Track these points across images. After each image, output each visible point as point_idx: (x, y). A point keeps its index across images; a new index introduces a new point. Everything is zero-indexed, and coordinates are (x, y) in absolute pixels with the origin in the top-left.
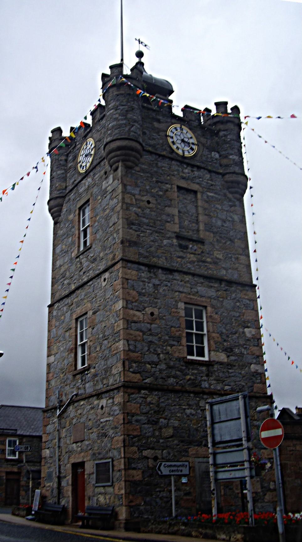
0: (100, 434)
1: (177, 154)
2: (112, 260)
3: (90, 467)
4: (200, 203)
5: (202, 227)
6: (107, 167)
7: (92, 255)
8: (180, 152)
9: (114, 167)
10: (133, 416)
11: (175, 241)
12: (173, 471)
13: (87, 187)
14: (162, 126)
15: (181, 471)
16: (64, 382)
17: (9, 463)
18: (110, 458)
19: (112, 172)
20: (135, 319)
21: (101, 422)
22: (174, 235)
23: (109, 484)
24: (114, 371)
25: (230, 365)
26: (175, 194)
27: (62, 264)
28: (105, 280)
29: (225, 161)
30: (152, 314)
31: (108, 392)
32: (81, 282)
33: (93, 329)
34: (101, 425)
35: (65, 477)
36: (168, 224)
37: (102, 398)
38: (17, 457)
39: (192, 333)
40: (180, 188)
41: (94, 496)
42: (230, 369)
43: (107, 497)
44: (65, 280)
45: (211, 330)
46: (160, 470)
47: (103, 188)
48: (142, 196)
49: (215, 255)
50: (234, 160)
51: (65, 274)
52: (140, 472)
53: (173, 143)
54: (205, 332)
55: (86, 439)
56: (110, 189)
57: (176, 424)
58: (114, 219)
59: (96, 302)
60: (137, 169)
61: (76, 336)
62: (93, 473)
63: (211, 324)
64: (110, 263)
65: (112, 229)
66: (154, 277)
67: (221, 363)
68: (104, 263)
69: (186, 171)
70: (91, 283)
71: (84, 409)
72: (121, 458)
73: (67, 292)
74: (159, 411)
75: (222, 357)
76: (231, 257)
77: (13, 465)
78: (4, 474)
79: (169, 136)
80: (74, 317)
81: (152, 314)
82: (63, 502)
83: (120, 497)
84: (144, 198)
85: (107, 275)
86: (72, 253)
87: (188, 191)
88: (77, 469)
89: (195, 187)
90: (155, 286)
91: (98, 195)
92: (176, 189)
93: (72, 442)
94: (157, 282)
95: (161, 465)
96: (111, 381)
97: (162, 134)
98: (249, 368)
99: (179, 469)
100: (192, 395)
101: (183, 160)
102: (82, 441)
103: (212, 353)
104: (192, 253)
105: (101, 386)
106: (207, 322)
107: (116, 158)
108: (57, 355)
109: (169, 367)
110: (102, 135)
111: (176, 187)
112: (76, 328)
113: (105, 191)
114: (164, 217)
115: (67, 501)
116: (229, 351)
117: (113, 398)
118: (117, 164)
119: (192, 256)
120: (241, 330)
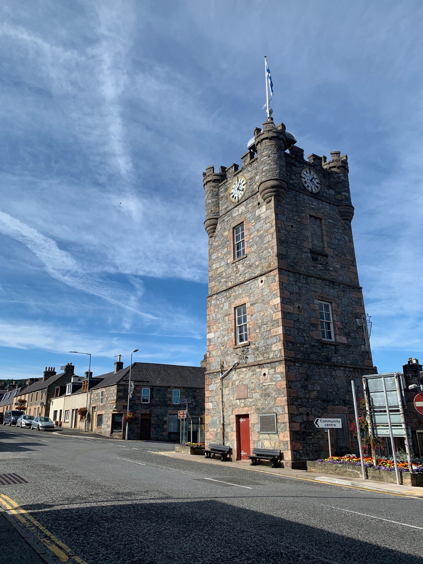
0: (263, 395)
1: (308, 191)
2: (267, 268)
3: (254, 419)
4: (324, 227)
5: (326, 245)
6: (261, 200)
7: (247, 263)
8: (310, 189)
9: (267, 200)
10: (292, 383)
11: (309, 255)
12: (327, 425)
13: (240, 212)
14: (297, 170)
15: (335, 425)
16: (225, 354)
17: (143, 407)
18: (274, 413)
19: (265, 203)
20: (288, 311)
21: (264, 386)
22: (309, 251)
23: (274, 432)
24: (274, 348)
25: (348, 346)
26: (307, 221)
27: (218, 267)
28: (262, 281)
29: (338, 197)
30: (299, 307)
31: (271, 363)
32: (237, 282)
33: (252, 316)
34: (264, 388)
35: (229, 424)
36: (305, 242)
37: (264, 367)
38: (149, 402)
39: (323, 322)
40: (311, 216)
41: (259, 441)
42: (349, 348)
43: (272, 443)
44: (222, 279)
45: (336, 320)
46: (317, 424)
47: (257, 214)
48: (288, 222)
49: (335, 265)
50: (345, 195)
51: (222, 274)
52: (298, 425)
53: (305, 182)
54: (332, 321)
55: (249, 396)
56: (263, 216)
57: (319, 388)
58: (269, 238)
59: (254, 297)
60: (284, 202)
61: (235, 320)
62: (46, 388)
63: (335, 315)
64: (265, 270)
65: (267, 245)
66: (298, 281)
67: (344, 344)
68: (259, 269)
69: (314, 203)
70: (248, 283)
71: (246, 374)
72: (285, 413)
73: (224, 288)
74: (308, 378)
75: (343, 340)
76: (345, 267)
77: (146, 408)
78: (140, 416)
79: (303, 177)
80: (233, 306)
81: (299, 307)
82: (227, 444)
83: (285, 443)
84: (290, 224)
85: (263, 278)
86: (227, 260)
87: (315, 217)
88: (239, 419)
89: (320, 216)
90: (300, 288)
91: (251, 220)
92: (308, 217)
93: (235, 399)
94: (301, 285)
95: (318, 420)
96: (271, 356)
97: (298, 175)
98: (361, 348)
99: (333, 423)
100: (327, 367)
101: (312, 194)
102: (245, 398)
103: (338, 337)
104: (321, 264)
105: (261, 358)
106: (333, 314)
107: (270, 194)
108: (217, 333)
109: (312, 346)
110: (253, 175)
111: (309, 216)
112: (235, 314)
113: (259, 217)
114: (302, 237)
115: (232, 443)
116: (347, 335)
117: (275, 368)
118: (270, 198)
119: (320, 265)
120: (354, 320)
